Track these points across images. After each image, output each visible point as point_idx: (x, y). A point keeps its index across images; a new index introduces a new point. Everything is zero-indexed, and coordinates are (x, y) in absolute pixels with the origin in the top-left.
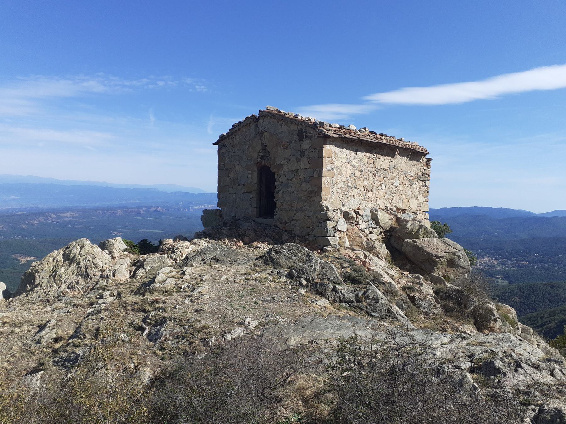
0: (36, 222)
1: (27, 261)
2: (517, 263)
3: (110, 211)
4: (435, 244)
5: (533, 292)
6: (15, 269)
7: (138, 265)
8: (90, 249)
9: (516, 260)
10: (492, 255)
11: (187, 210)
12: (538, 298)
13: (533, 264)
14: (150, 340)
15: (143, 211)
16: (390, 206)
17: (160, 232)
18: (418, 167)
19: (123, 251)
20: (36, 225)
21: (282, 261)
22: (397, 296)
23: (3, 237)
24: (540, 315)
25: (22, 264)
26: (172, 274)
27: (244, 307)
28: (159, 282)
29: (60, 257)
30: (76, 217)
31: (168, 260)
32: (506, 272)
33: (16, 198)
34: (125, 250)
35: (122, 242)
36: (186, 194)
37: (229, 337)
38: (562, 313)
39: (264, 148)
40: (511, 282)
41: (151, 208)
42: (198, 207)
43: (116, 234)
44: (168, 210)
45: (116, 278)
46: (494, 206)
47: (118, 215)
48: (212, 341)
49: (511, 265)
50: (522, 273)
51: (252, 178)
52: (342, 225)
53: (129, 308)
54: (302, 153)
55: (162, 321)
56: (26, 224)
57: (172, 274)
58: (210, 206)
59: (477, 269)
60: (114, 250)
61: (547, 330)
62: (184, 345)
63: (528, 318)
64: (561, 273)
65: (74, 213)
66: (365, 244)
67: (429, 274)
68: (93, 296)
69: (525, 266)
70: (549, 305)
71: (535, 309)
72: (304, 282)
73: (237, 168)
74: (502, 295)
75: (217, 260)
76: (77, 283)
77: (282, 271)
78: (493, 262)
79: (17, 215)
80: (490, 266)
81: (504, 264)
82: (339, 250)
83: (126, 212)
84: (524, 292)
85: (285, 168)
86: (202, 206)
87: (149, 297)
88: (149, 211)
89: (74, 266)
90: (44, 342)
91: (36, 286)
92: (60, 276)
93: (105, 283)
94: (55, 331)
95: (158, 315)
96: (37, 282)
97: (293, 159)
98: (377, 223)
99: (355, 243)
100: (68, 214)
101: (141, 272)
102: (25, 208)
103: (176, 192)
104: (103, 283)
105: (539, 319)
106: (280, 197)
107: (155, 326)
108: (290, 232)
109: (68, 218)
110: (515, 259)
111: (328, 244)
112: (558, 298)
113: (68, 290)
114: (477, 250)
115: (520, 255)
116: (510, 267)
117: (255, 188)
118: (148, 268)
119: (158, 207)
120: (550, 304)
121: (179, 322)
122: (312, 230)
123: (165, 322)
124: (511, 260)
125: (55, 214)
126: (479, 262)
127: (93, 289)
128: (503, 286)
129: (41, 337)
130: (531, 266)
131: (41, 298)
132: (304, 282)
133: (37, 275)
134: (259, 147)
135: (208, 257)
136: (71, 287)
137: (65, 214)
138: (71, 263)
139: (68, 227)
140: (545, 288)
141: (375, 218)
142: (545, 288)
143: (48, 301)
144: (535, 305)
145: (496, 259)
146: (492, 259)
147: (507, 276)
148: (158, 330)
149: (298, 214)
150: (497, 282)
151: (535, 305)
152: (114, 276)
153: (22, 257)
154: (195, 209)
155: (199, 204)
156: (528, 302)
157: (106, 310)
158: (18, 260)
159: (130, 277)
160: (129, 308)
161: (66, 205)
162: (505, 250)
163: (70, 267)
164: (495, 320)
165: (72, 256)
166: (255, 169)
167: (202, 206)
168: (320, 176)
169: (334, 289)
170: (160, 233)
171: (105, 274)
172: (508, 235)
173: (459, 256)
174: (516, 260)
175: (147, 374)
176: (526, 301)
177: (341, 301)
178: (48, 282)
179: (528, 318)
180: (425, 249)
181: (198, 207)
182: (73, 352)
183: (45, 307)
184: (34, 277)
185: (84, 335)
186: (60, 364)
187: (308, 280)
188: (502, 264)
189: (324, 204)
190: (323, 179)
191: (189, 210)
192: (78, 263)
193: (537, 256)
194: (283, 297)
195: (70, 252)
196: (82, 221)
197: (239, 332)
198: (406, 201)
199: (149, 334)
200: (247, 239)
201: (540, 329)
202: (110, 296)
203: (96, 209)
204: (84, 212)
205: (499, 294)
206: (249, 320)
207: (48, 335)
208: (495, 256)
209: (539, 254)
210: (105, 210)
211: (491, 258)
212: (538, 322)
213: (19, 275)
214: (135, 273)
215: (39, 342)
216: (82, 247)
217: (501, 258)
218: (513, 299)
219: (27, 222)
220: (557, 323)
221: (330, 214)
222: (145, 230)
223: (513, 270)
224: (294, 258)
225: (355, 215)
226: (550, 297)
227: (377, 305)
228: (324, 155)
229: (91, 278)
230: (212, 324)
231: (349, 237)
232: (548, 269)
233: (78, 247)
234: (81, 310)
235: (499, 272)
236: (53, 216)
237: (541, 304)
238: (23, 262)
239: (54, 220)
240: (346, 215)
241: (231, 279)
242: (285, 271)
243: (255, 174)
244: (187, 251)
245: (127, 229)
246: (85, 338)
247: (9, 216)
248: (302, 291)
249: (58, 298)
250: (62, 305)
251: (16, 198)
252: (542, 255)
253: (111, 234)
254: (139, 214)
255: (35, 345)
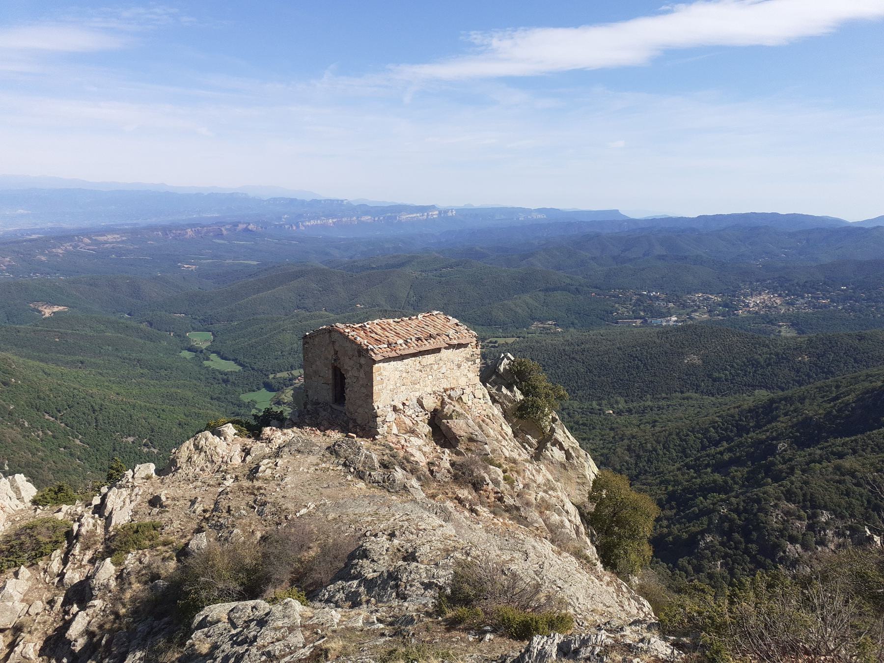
0: (60, 251)
1: (54, 313)
2: (813, 302)
3: (174, 231)
4: (461, 425)
5: (830, 348)
6: (37, 325)
7: (246, 451)
8: (212, 440)
9: (812, 297)
10: (774, 290)
11: (294, 228)
12: (837, 356)
13: (838, 302)
14: (259, 515)
15: (226, 230)
16: (437, 389)
17: (255, 263)
18: (465, 352)
19: (234, 435)
20: (61, 255)
21: (342, 452)
22: (418, 471)
23: (11, 276)
24: (835, 384)
25: (44, 319)
26: (269, 465)
27: (310, 493)
28: (261, 471)
29: (192, 447)
30: (122, 242)
31: (266, 449)
32: (795, 316)
33: (26, 212)
34: (235, 434)
35: (233, 428)
36: (292, 201)
37: (298, 515)
38: (869, 379)
39: (336, 353)
40: (801, 332)
41: (238, 226)
42: (312, 222)
43: (188, 267)
44: (265, 228)
45: (232, 463)
46: (783, 211)
47: (187, 236)
48: (290, 517)
49: (802, 306)
50: (818, 318)
51: (329, 374)
52: (391, 416)
53: (245, 491)
54: (361, 366)
55: (264, 504)
56: (46, 255)
57: (269, 465)
58: (330, 221)
59: (749, 312)
60: (227, 437)
61: (842, 405)
62: (276, 519)
63: (816, 388)
64: (879, 316)
65: (118, 236)
66: (408, 429)
67: (455, 448)
68: (219, 476)
69: (825, 306)
70: (853, 367)
71: (832, 373)
72: (352, 470)
73: (318, 363)
74: (784, 353)
75: (299, 452)
76: (207, 467)
77: (340, 461)
78: (774, 301)
79: (31, 241)
80: (770, 308)
81: (792, 304)
82: (386, 437)
83: (198, 232)
84: (817, 348)
85: (350, 373)
86: (319, 221)
87: (257, 484)
88: (235, 230)
89: (203, 454)
90: (197, 512)
91: (179, 469)
92: (194, 462)
93: (225, 468)
94: (202, 505)
95: (262, 499)
96: (178, 466)
97: (355, 368)
98: (423, 407)
99: (401, 428)
100: (110, 238)
101: (249, 458)
102: (41, 229)
103: (275, 199)
104: (224, 467)
105: (833, 389)
106: (348, 393)
107: (261, 506)
108: (355, 421)
109: (111, 243)
110: (810, 295)
111: (378, 434)
112: (868, 357)
113: (201, 472)
114: (751, 283)
115: (817, 290)
116: (801, 308)
117: (331, 382)
118: (254, 455)
119: (249, 224)
120: (856, 365)
121: (274, 504)
122: (369, 422)
123: (266, 504)
124: (803, 298)
125: (90, 239)
126: (754, 301)
127: (218, 471)
128: (786, 338)
129: (195, 510)
130: (834, 307)
131: (184, 478)
132: (352, 470)
133: (178, 460)
134: (332, 352)
135: (293, 448)
136: (202, 470)
137: (105, 238)
138: (200, 452)
139: (111, 259)
140: (850, 341)
141: (420, 403)
142: (850, 341)
143: (189, 480)
144: (833, 367)
145: (780, 295)
146: (774, 297)
147: (795, 323)
148: (263, 509)
149: (360, 409)
150: (780, 332)
151: (833, 367)
152: (231, 461)
153: (45, 307)
154: (308, 226)
155: (313, 219)
156: (823, 362)
157: (231, 492)
158: (40, 312)
159: (242, 462)
160: (245, 491)
161: (103, 223)
162: (796, 281)
163: (200, 455)
164: (488, 484)
165: (200, 447)
166: (330, 367)
167: (319, 221)
168: (372, 386)
169: (370, 475)
170: (254, 265)
171: (225, 460)
172: (802, 257)
173: (476, 435)
174: (812, 297)
175: (259, 535)
176: (820, 361)
177: (373, 483)
178: (187, 466)
179: (816, 388)
180: (453, 429)
181: (312, 222)
182: (218, 521)
183: (188, 484)
184: (176, 462)
185: (222, 510)
186: (213, 527)
187: (354, 469)
188: (788, 304)
189: (375, 406)
190: (374, 388)
191: (298, 227)
192: (205, 452)
193: (845, 290)
194: (336, 483)
195: (199, 443)
196: (132, 247)
197: (304, 511)
198: (455, 381)
199: (258, 511)
200: (322, 428)
201: (832, 404)
202: (231, 478)
203: (152, 228)
204: (135, 233)
205: (779, 351)
206: (310, 504)
207: (199, 508)
208: (779, 292)
209: (847, 287)
210: (166, 229)
211: (773, 294)
212: (831, 393)
213: (44, 335)
214: (245, 458)
215: (194, 512)
216: (206, 439)
217: (787, 295)
218: (800, 359)
219: (47, 252)
220: (857, 396)
221: (379, 412)
222: (231, 261)
223: (805, 313)
224: (350, 450)
225: (402, 407)
226: (857, 354)
227: (395, 484)
228: (374, 371)
229: (215, 463)
230: (291, 506)
231: (397, 424)
232: (860, 311)
233: (204, 439)
234: (212, 489)
235: (783, 317)
236: (87, 240)
237: (842, 365)
238: (47, 315)
239: (88, 247)
240: (395, 409)
241: (306, 470)
242: (342, 461)
243: (331, 371)
244: (280, 441)
245: (201, 259)
246: (222, 512)
247: (17, 242)
248: (349, 477)
249: (196, 478)
250: (199, 484)
251: (26, 212)
252: (852, 289)
253: (179, 267)
254: (220, 235)
255: (192, 514)
